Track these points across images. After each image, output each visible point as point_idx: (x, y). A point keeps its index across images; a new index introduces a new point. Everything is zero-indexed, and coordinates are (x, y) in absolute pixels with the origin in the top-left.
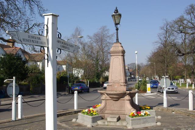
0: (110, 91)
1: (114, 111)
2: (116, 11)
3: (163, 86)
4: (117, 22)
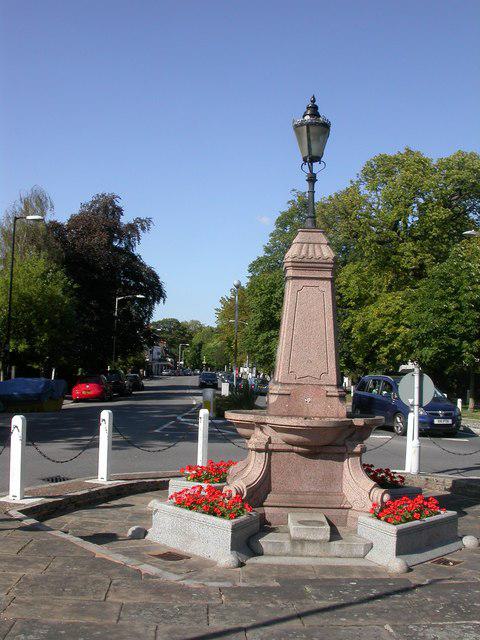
0: (283, 416)
1: (300, 497)
2: (314, 110)
3: (411, 401)
4: (314, 152)
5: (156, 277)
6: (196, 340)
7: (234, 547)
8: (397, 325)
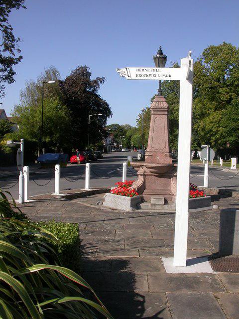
1: (156, 191)
2: (161, 52)
5: (107, 105)
6: (128, 134)
7: (132, 206)
8: (219, 127)
